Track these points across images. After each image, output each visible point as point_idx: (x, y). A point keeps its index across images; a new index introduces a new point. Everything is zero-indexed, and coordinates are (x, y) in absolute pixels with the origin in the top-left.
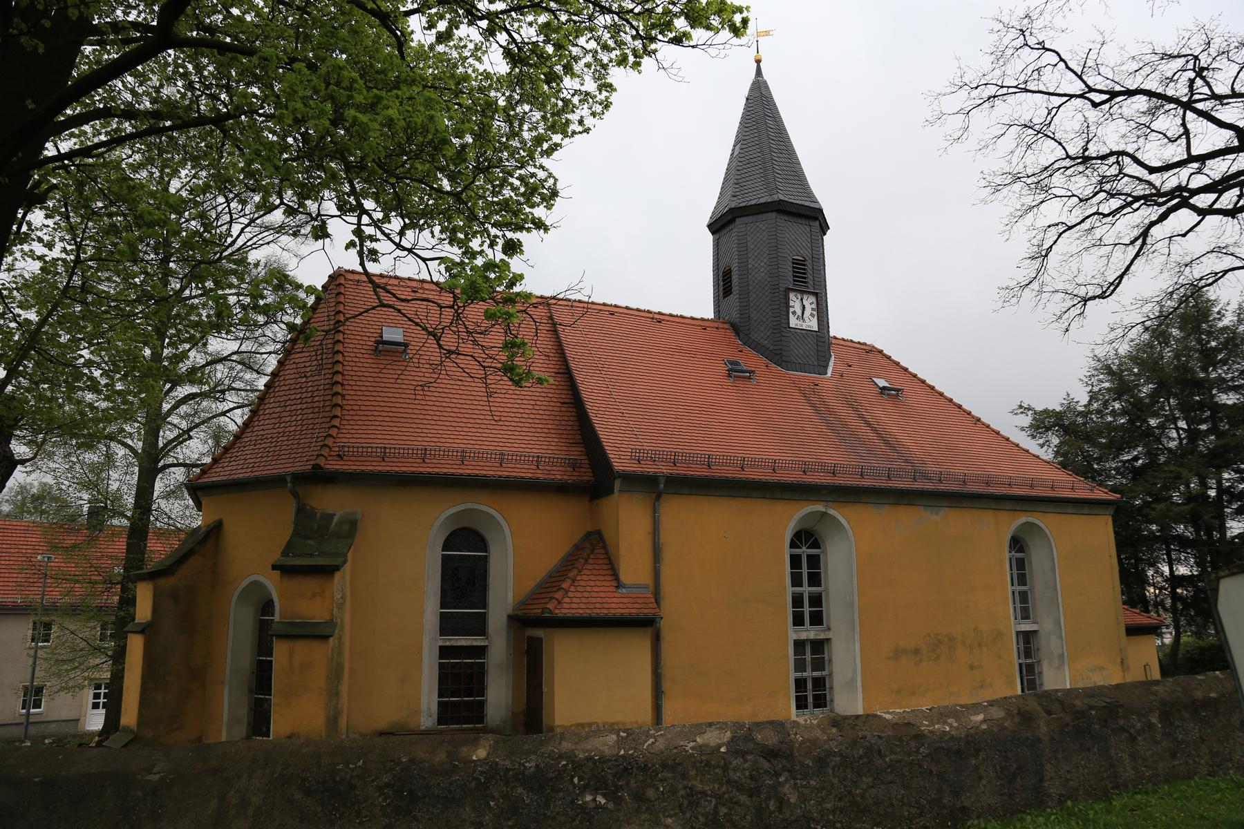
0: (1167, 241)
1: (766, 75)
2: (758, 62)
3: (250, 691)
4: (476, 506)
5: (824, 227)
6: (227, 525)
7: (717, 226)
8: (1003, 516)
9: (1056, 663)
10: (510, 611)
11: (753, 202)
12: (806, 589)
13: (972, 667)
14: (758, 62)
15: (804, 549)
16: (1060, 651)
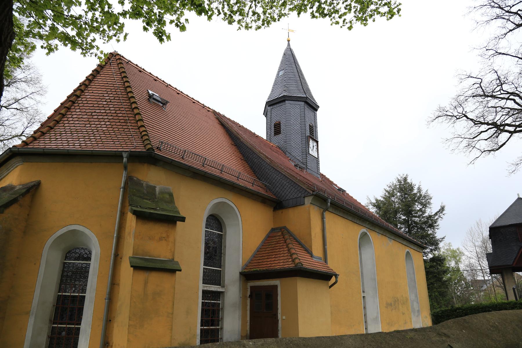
1: (292, 47)
2: (289, 41)
3: (50, 321)
4: (227, 201)
6: (46, 186)
9: (416, 314)
10: (241, 270)
11: (295, 95)
14: (289, 41)
16: (418, 309)
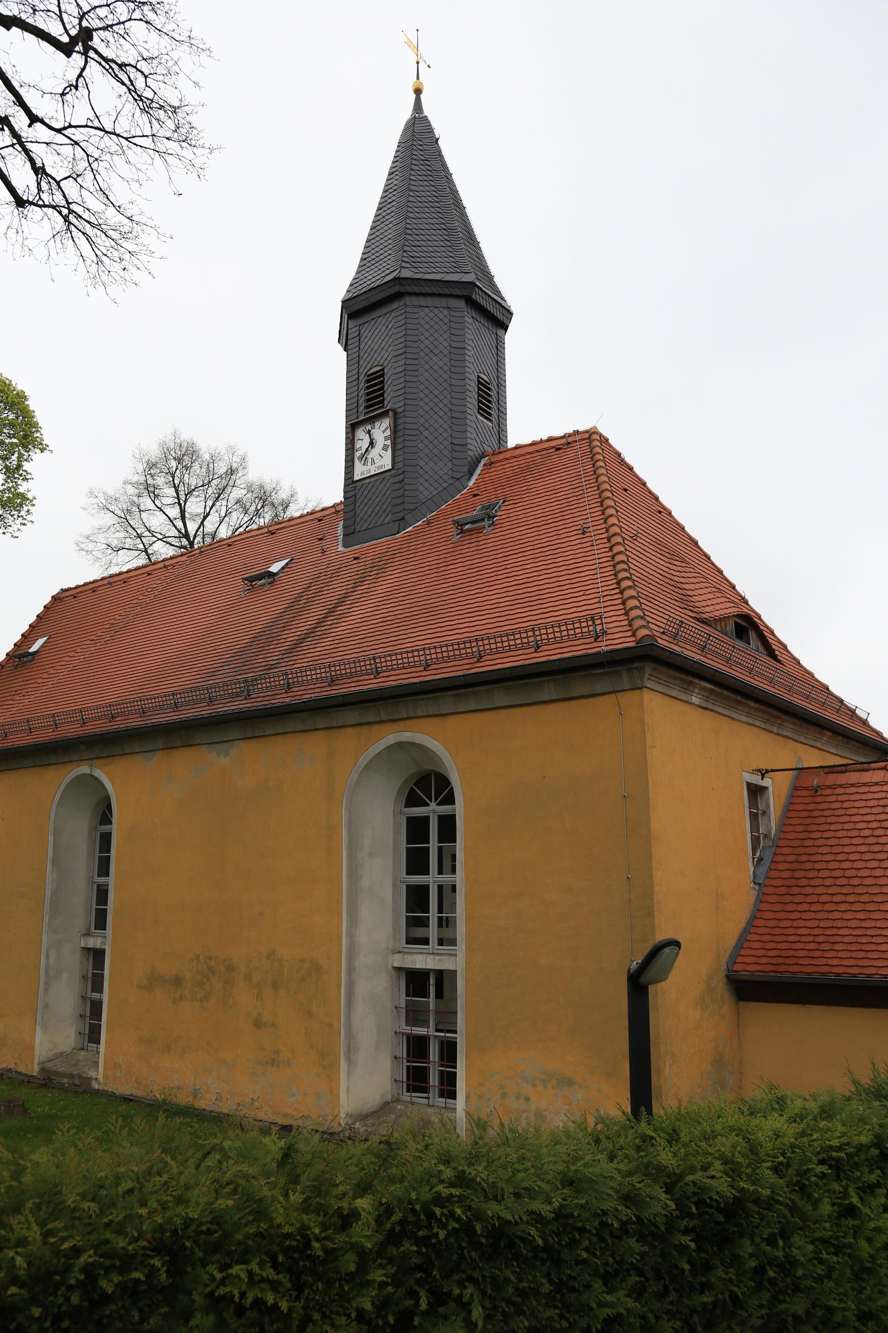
0: (83, 190)
1: (427, 111)
2: (418, 92)
5: (497, 318)
7: (358, 309)
8: (347, 740)
12: (432, 879)
13: (258, 1024)
14: (418, 92)
15: (433, 806)
